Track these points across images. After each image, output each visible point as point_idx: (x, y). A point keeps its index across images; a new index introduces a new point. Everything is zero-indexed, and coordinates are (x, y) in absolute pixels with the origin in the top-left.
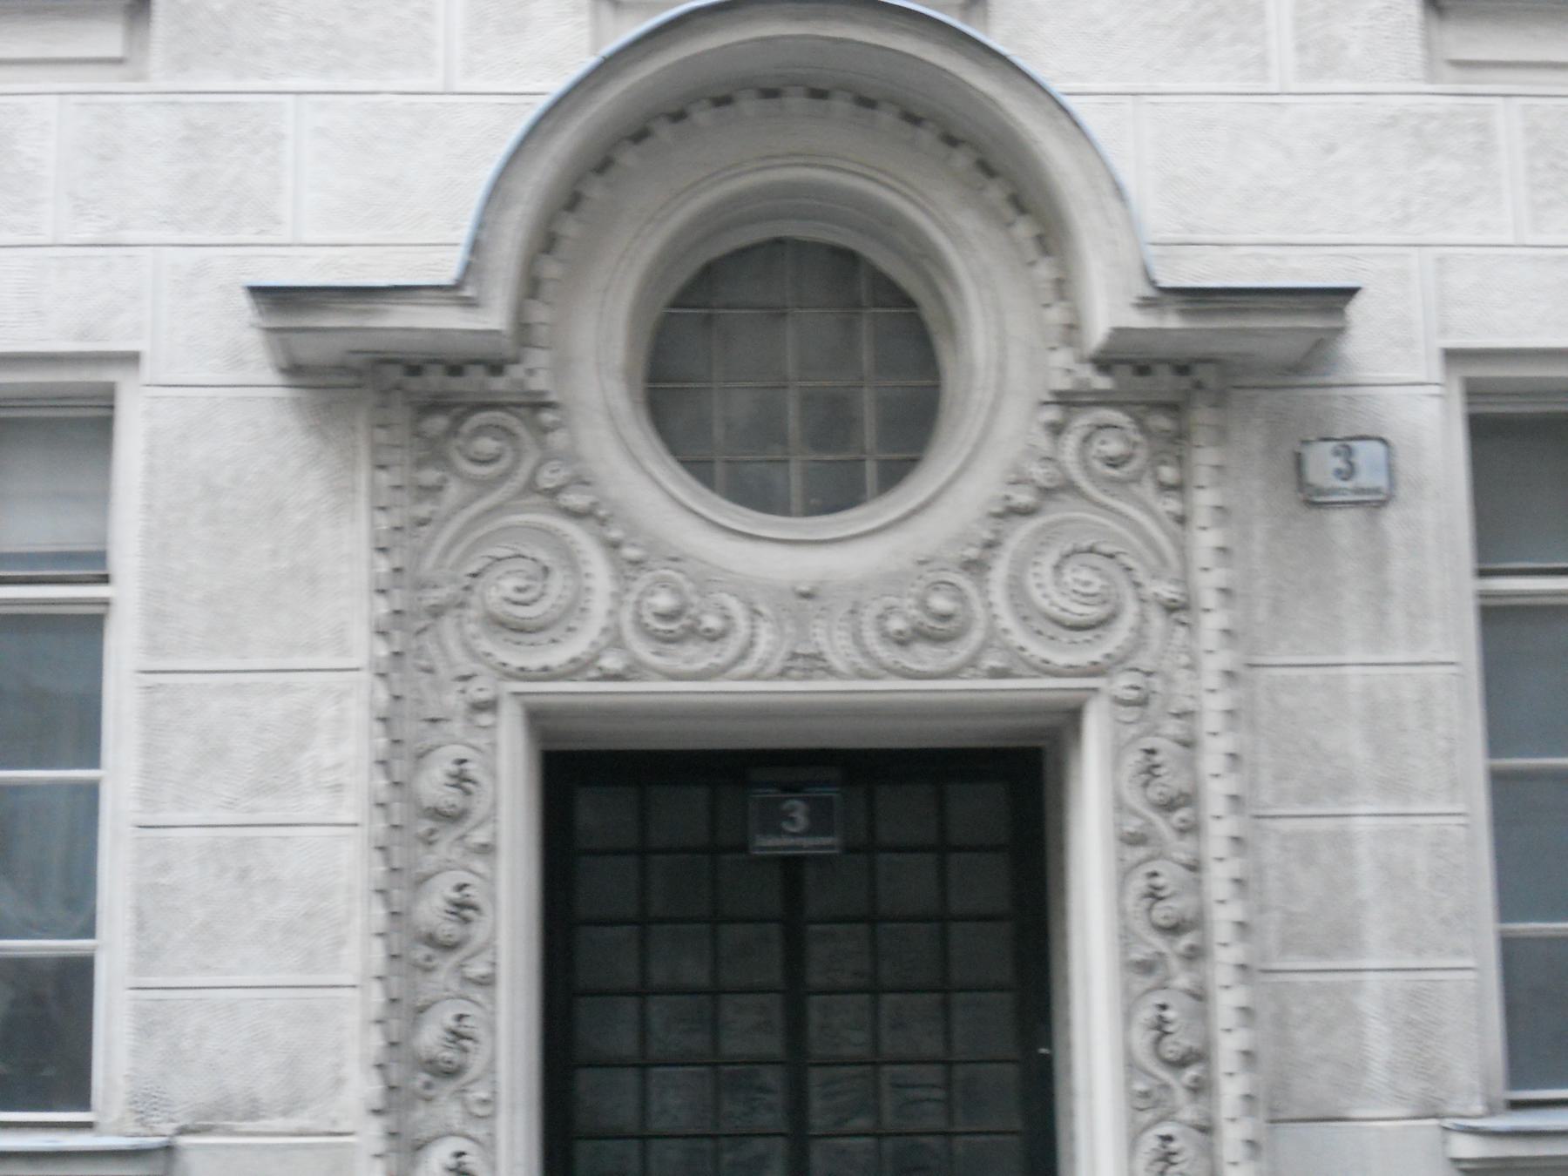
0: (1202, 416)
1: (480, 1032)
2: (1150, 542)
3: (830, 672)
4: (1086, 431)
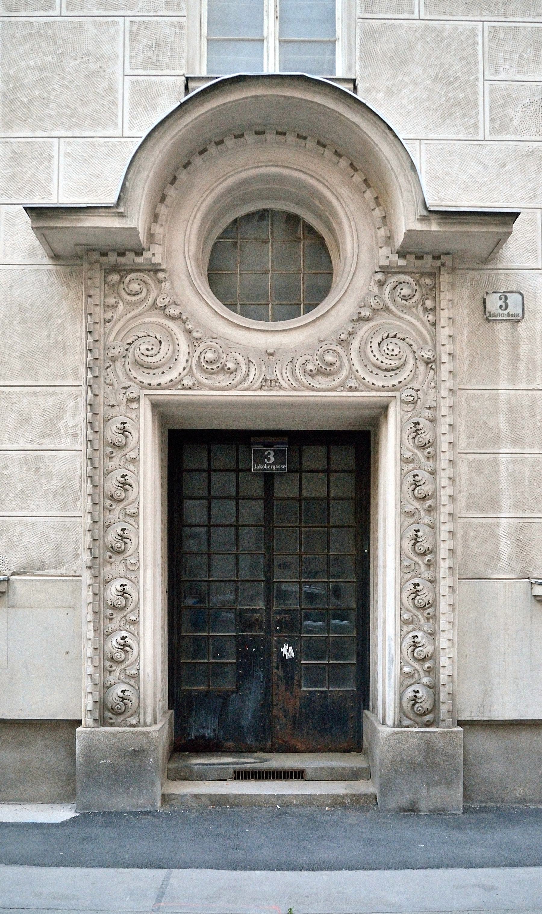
0: (445, 278)
1: (132, 536)
2: (420, 334)
3: (281, 388)
4: (395, 284)
